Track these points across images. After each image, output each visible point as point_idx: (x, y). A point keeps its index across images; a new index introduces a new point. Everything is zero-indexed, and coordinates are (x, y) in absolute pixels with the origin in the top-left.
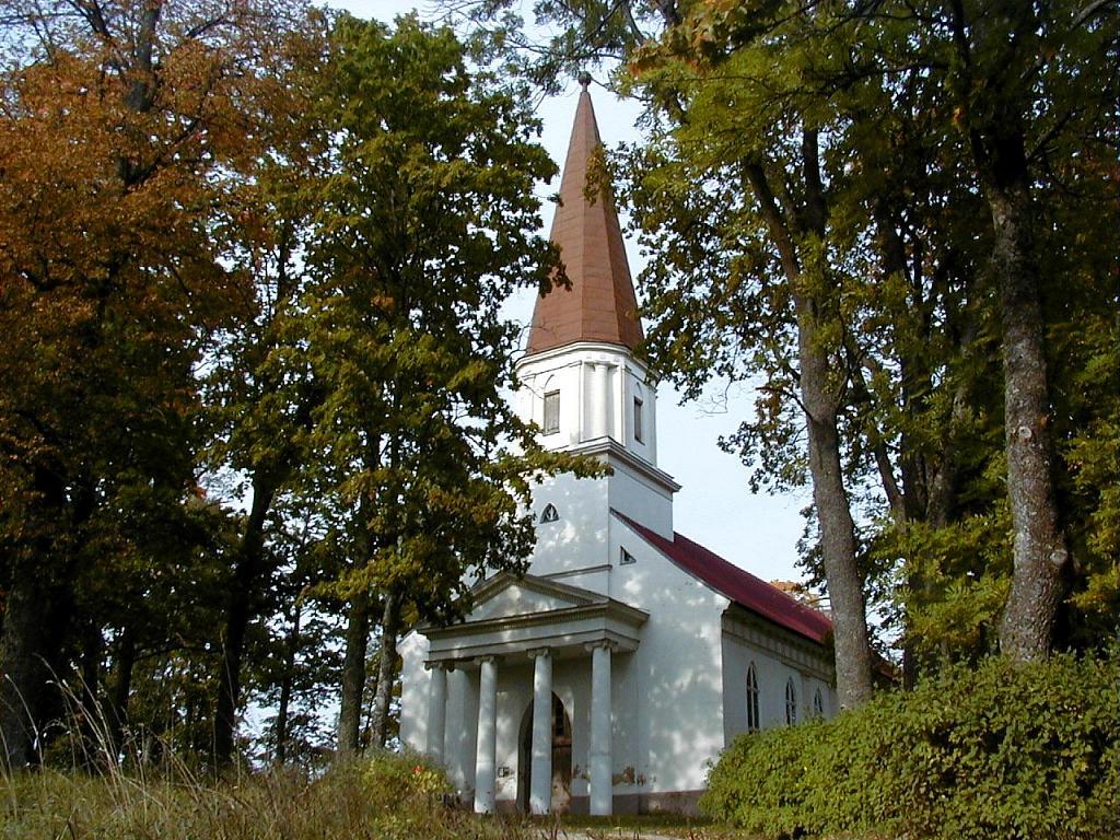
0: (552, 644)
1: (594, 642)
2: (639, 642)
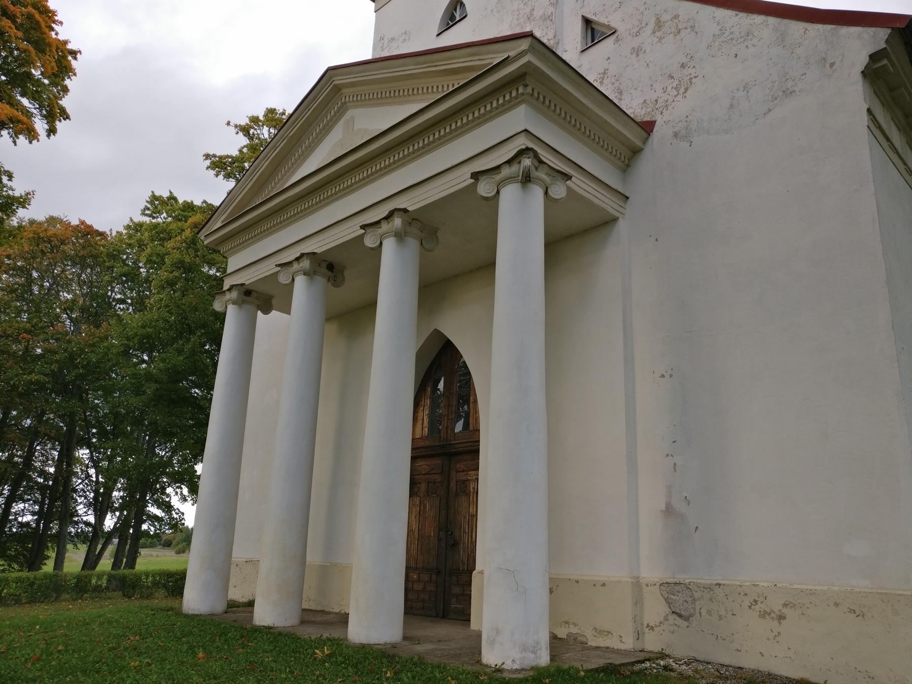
1: (498, 168)
2: (627, 198)
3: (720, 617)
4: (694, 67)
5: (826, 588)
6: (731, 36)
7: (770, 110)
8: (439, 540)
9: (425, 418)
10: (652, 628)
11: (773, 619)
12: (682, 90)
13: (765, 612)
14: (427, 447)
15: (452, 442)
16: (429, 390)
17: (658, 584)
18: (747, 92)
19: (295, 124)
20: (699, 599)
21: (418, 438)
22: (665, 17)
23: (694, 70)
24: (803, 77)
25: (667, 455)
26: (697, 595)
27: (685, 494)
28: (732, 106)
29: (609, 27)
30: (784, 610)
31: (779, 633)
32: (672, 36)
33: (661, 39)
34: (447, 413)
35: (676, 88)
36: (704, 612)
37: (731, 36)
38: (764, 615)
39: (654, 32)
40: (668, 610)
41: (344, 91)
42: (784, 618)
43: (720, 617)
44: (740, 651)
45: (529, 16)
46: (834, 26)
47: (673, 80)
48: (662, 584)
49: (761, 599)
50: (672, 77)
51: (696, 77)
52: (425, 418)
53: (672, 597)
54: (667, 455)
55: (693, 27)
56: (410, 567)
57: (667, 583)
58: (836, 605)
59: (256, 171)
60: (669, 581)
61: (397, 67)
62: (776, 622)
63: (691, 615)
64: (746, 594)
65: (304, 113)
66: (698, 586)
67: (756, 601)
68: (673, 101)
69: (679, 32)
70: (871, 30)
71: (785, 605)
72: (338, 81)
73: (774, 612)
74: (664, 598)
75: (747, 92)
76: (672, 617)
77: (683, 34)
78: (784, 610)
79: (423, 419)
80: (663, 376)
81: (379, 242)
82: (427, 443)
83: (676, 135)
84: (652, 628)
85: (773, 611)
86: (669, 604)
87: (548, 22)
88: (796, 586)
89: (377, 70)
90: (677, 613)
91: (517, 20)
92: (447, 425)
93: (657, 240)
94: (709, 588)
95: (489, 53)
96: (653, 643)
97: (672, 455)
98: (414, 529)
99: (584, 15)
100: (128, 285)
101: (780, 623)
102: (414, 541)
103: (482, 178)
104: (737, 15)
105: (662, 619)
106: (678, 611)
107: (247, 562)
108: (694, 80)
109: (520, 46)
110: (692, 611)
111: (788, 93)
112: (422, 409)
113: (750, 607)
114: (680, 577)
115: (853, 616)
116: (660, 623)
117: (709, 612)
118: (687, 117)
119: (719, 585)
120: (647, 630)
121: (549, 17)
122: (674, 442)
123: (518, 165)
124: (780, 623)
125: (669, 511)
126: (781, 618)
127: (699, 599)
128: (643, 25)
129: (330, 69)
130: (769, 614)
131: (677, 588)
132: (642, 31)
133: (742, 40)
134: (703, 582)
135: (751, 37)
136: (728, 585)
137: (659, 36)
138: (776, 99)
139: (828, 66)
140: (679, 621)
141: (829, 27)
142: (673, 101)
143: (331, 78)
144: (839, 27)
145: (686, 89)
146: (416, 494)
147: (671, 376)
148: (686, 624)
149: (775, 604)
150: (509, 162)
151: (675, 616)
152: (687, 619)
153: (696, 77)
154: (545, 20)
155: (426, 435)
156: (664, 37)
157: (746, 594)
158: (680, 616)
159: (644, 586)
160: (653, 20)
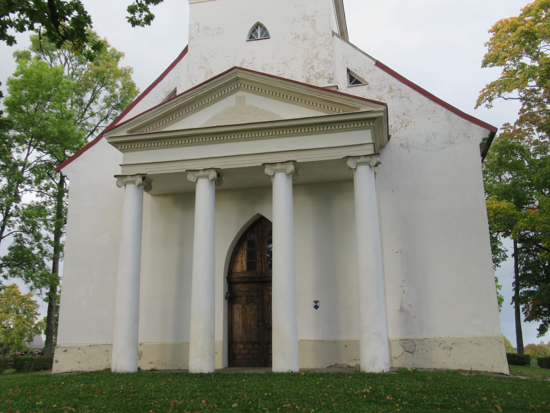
0: (301, 158)
1: (359, 157)
3: (427, 351)
4: (410, 116)
5: (467, 336)
6: (426, 109)
7: (444, 148)
8: (258, 327)
9: (244, 261)
10: (396, 358)
11: (448, 349)
12: (404, 125)
13: (445, 347)
14: (249, 278)
15: (268, 276)
16: (246, 245)
17: (398, 340)
18: (435, 136)
19: (203, 90)
20: (417, 345)
21: (239, 272)
22: (394, 88)
23: (409, 118)
24: (458, 138)
25: (400, 286)
26: (416, 343)
27: (409, 303)
28: (427, 140)
29: (366, 82)
30: (453, 346)
31: (450, 354)
32: (398, 98)
33: (392, 97)
34: (260, 259)
35: (401, 123)
36: (420, 350)
37: (426, 109)
38: (444, 348)
39: (389, 92)
40: (403, 350)
41: (240, 81)
42: (452, 349)
43: (427, 351)
44: (435, 362)
45: (316, 56)
46: (469, 122)
47: (399, 119)
48: (400, 340)
49: (443, 342)
50: (399, 118)
51: (411, 121)
52: (244, 261)
53: (405, 345)
54: (400, 286)
55: (408, 98)
56: (237, 342)
57: (403, 339)
58: (471, 342)
59: (166, 108)
60: (403, 338)
61: (295, 87)
62: (449, 351)
63: (414, 351)
64: (437, 341)
65: (211, 86)
66: (417, 340)
67: (441, 344)
68: (400, 129)
69: (402, 97)
70: (483, 129)
71: (452, 344)
72: (240, 75)
73: (448, 347)
74: (402, 346)
75: (435, 136)
76: (405, 353)
77: (403, 98)
78: (452, 346)
79: (242, 262)
80: (397, 252)
81: (274, 173)
82: (246, 275)
83: (401, 145)
84: (396, 358)
85: (448, 347)
86: (404, 348)
87: (329, 64)
88: (456, 337)
89: (276, 82)
90: (407, 351)
91: (307, 55)
92: (262, 266)
93: (393, 191)
94: (422, 340)
95: (359, 103)
96: (397, 364)
97: (402, 286)
98: (238, 321)
99: (349, 68)
100: (532, 248)
101: (450, 350)
102: (239, 328)
103: (350, 159)
104: (429, 101)
105: (401, 354)
106: (408, 350)
107: (90, 346)
108: (409, 122)
109: (379, 107)
110: (414, 350)
111: (452, 143)
112: (241, 256)
113: (439, 346)
114: (407, 337)
115: (477, 345)
116: (400, 356)
117: (422, 350)
118: (407, 138)
119: (426, 339)
120: (394, 359)
121: (329, 62)
122: (403, 281)
123: (370, 158)
124: (450, 350)
125: (402, 310)
126: (451, 349)
127: (417, 345)
128: (383, 87)
129: (235, 68)
130: (446, 348)
131: (407, 341)
132: (382, 90)
133: (431, 113)
134: (418, 338)
135: (435, 113)
136: (430, 338)
137: (392, 95)
138: (447, 143)
139: (467, 137)
140: (408, 354)
141: (468, 121)
142: (400, 129)
143: (236, 72)
144: (471, 123)
145: (406, 126)
146: (238, 303)
147: (401, 252)
148: (412, 355)
149: (449, 344)
150: (366, 156)
151: (407, 353)
152: (412, 353)
153: (411, 121)
154: (326, 62)
155: (245, 270)
156: (394, 97)
157: (437, 341)
158: (409, 352)
159: (392, 341)
160: (388, 87)
